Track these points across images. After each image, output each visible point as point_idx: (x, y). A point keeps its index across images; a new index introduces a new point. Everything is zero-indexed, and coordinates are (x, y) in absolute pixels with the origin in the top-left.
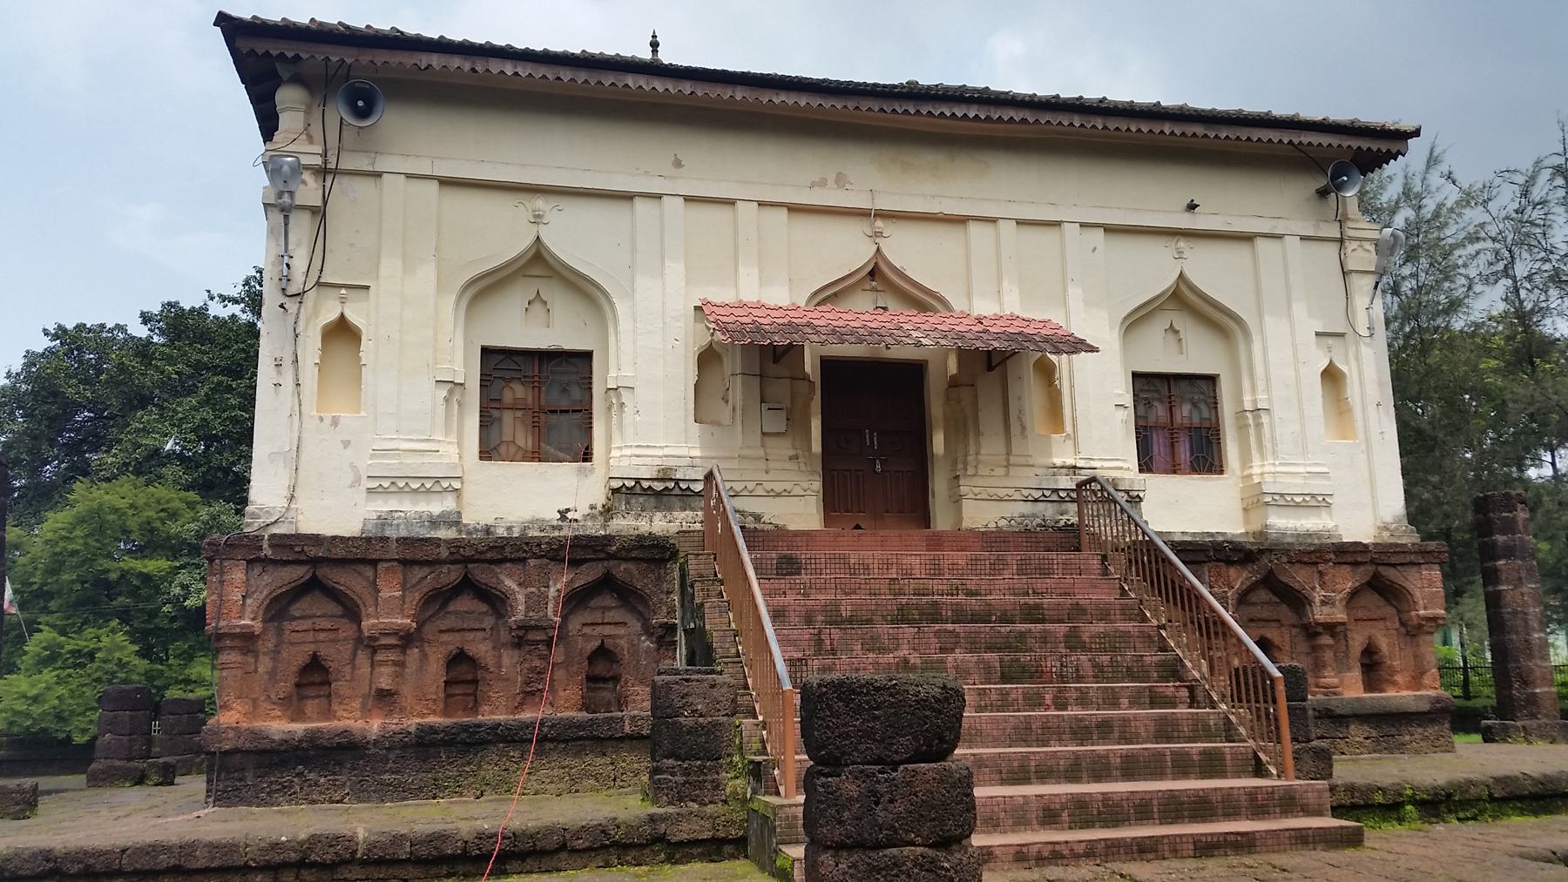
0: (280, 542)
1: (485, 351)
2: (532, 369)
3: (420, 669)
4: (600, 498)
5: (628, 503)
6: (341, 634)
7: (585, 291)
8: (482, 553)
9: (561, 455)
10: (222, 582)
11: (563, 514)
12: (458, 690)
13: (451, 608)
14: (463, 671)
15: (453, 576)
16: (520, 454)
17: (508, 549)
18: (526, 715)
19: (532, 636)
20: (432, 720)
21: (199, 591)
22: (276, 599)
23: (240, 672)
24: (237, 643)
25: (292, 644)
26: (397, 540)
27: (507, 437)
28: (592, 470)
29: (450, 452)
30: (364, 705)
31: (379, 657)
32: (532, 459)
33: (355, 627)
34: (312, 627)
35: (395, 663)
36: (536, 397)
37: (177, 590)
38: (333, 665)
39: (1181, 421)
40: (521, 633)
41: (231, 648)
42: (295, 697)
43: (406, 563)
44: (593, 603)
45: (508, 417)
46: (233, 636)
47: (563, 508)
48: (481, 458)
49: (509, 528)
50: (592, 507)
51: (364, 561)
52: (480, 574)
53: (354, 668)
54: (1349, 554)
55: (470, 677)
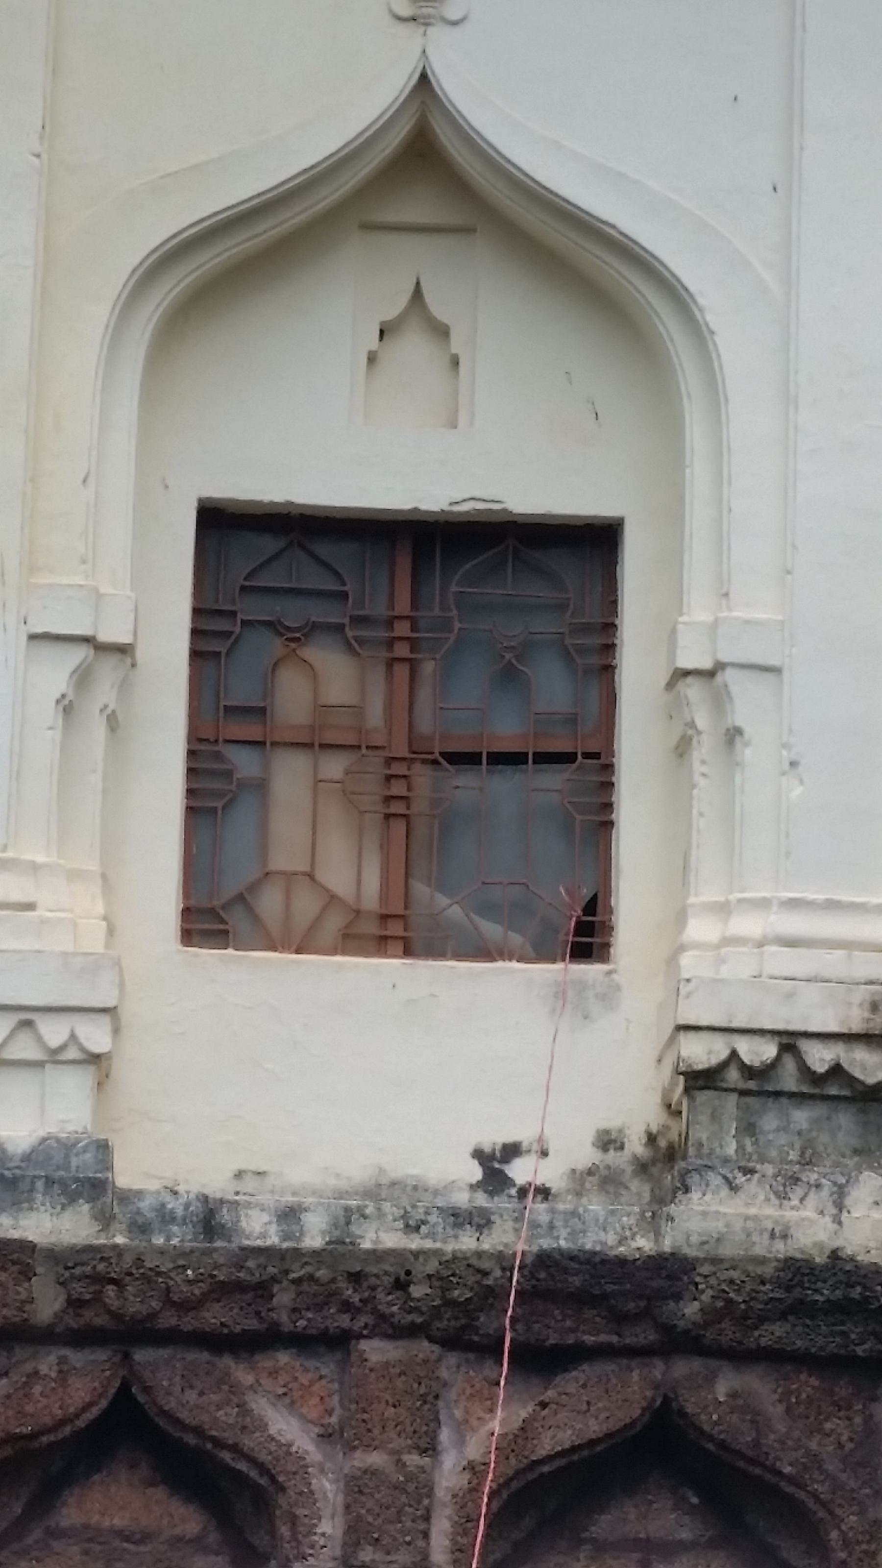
1: (220, 524)
2: (387, 591)
4: (635, 1102)
5: (748, 1129)
7: (590, 276)
8: (185, 1306)
9: (491, 930)
11: (494, 1164)
13: (71, 1513)
15: (79, 1392)
16: (334, 923)
17: (283, 1297)
27: (287, 855)
28: (609, 996)
29: (72, 916)
32: (380, 945)
44: (604, 1525)
45: (291, 779)
47: (494, 1137)
48: (188, 936)
49: (289, 1215)
50: (608, 1141)
52: (179, 1388)
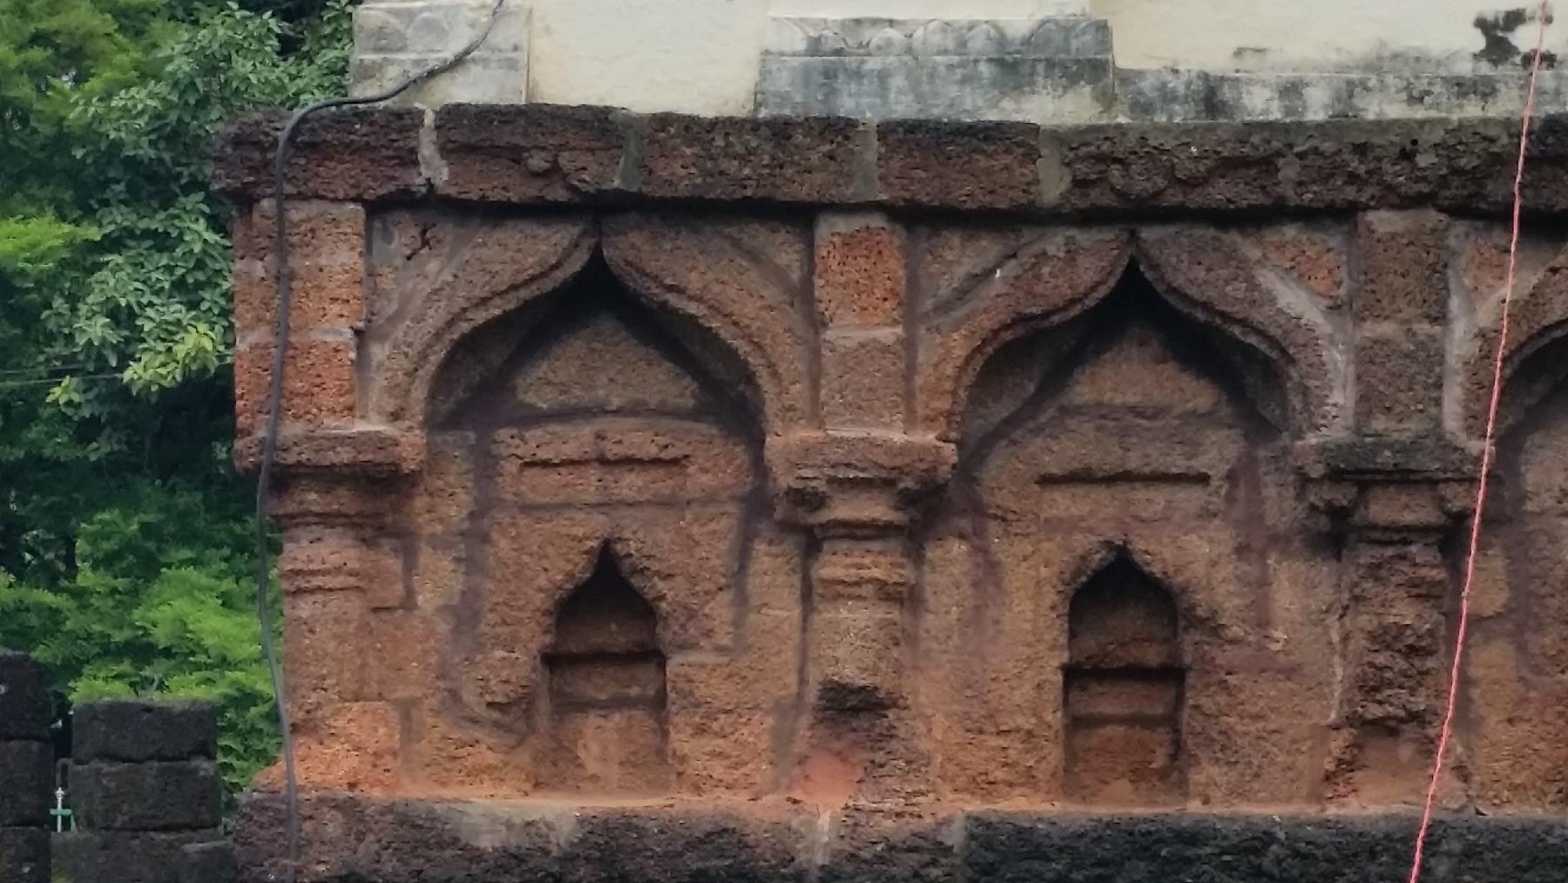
0: (480, 133)
3: (975, 618)
6: (698, 480)
8: (1190, 183)
10: (284, 279)
11: (1497, 35)
12: (1108, 702)
13: (1082, 391)
14: (1128, 634)
17: (1289, 171)
18: (1368, 804)
19: (1385, 509)
20: (1020, 805)
21: (170, 332)
22: (469, 346)
23: (354, 606)
24: (344, 500)
25: (527, 509)
26: (886, 130)
30: (782, 739)
31: (834, 565)
33: (741, 454)
34: (603, 456)
35: (889, 594)
37: (97, 329)
38: (670, 593)
40: (1341, 495)
41: (326, 519)
42: (544, 705)
43: (918, 218)
46: (328, 476)
49: (1291, 90)
52: (1188, 266)
53: (742, 600)
55: (1153, 656)
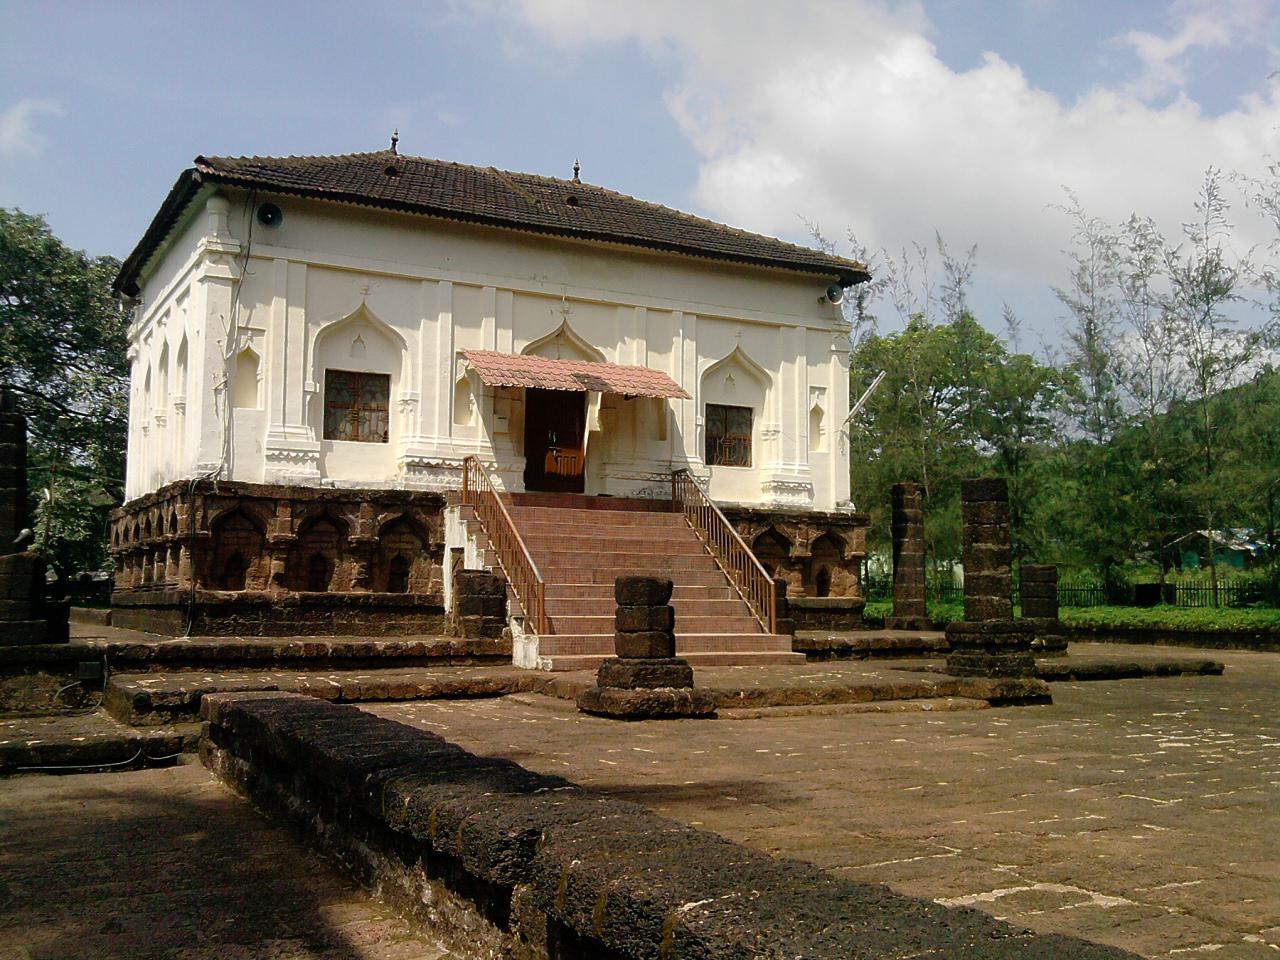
13: (315, 528)
36: (352, 400)
39: (728, 434)
51: (270, 499)
54: (817, 519)
